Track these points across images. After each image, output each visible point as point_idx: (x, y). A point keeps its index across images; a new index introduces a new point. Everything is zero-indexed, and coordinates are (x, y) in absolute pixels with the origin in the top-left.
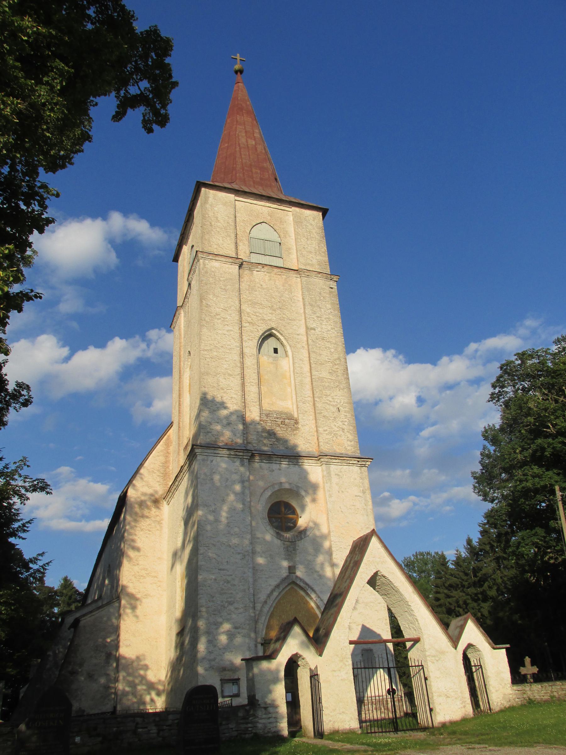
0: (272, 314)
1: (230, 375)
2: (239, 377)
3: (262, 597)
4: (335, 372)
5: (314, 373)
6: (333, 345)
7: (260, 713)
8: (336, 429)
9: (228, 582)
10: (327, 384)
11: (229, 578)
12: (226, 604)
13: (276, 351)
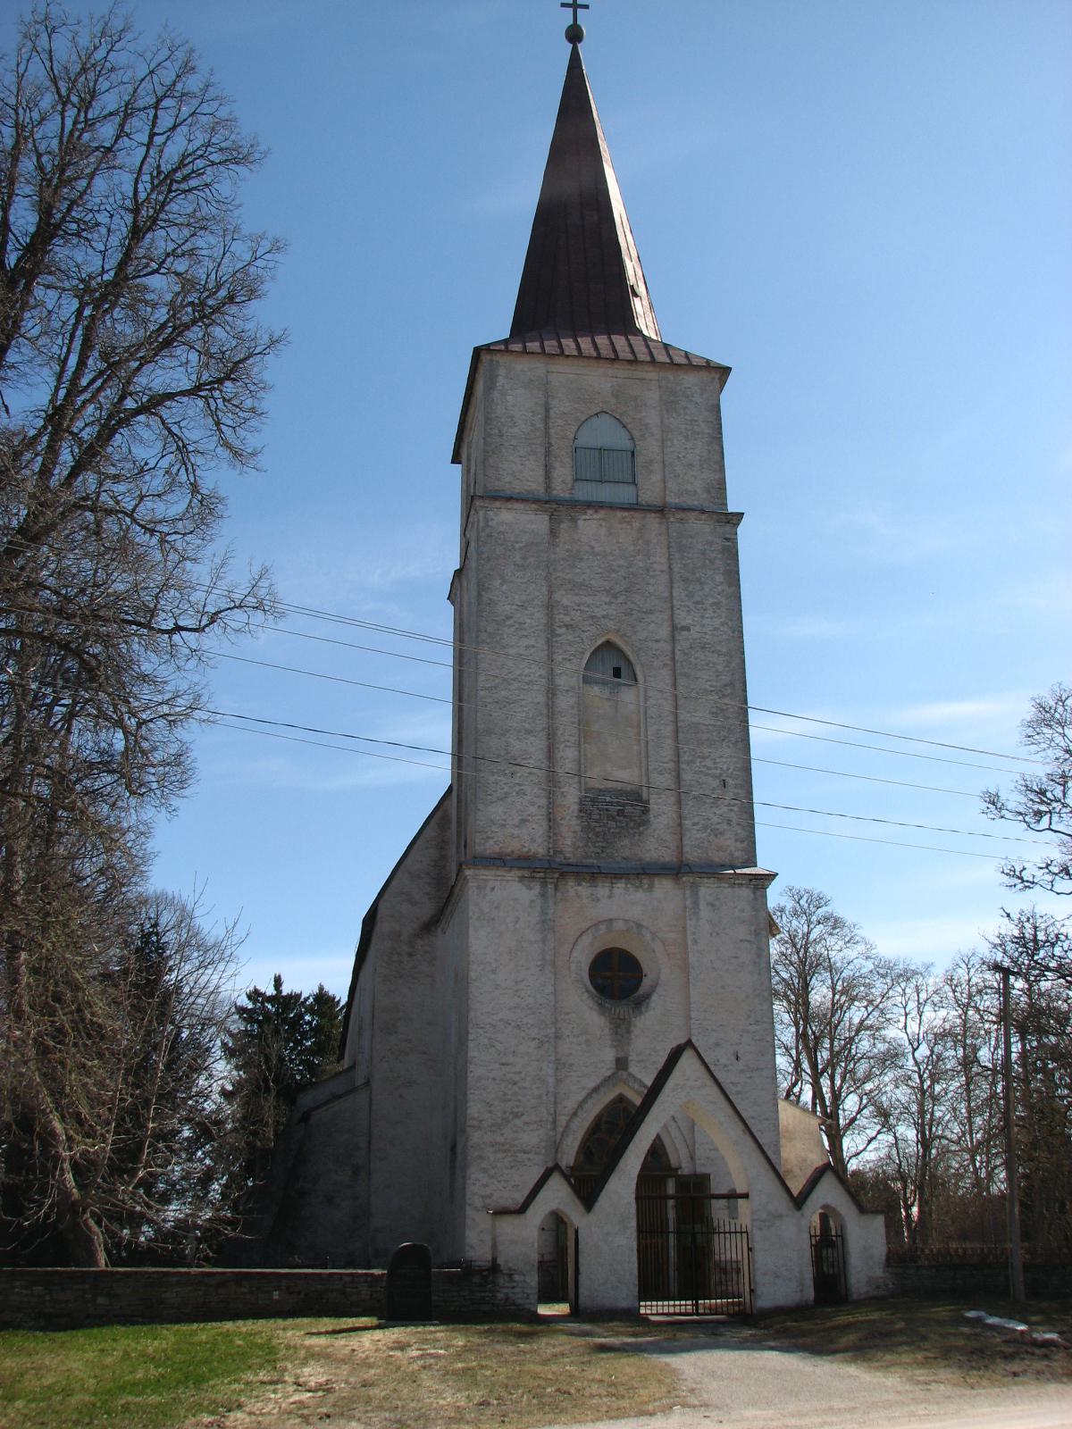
0: (610, 603)
1: (529, 732)
3: (571, 1104)
4: (722, 710)
5: (683, 716)
7: (501, 1280)
9: (515, 1083)
10: (705, 737)
11: (517, 1078)
12: (511, 1117)
13: (617, 673)
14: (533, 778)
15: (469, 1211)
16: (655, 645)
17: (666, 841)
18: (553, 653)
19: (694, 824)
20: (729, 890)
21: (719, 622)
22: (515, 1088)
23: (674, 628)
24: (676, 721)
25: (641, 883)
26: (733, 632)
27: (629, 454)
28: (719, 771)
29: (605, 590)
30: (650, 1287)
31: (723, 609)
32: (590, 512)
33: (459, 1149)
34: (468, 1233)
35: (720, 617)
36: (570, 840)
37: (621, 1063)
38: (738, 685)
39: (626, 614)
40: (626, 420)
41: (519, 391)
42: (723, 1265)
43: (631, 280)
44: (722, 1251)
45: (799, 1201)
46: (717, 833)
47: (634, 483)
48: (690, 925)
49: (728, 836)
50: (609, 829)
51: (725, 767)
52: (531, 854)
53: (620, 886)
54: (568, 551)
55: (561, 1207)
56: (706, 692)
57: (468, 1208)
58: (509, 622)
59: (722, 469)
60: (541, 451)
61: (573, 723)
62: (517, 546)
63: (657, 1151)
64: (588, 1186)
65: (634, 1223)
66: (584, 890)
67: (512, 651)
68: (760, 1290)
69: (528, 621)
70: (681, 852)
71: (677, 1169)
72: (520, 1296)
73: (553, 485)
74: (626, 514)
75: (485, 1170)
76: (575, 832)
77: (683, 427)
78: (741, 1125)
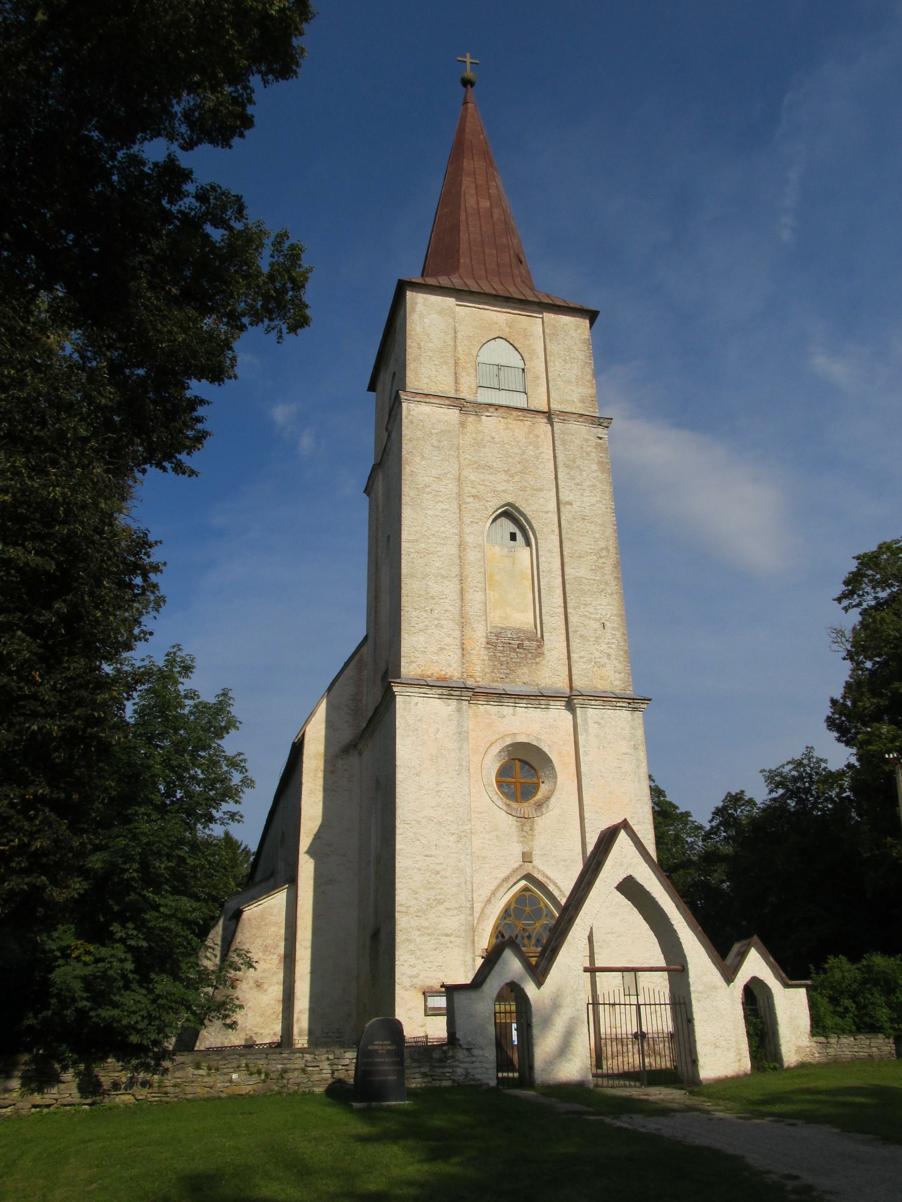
0: (508, 481)
1: (444, 577)
2: (456, 580)
3: (486, 892)
4: (601, 568)
6: (598, 528)
8: (598, 654)
10: (587, 588)
11: (439, 868)
19: (581, 657)
22: (438, 877)
37: (527, 857)
49: (608, 668)
54: (474, 439)
57: (397, 987)
58: (427, 490)
60: (451, 362)
67: (430, 513)
74: (520, 413)
75: (412, 952)
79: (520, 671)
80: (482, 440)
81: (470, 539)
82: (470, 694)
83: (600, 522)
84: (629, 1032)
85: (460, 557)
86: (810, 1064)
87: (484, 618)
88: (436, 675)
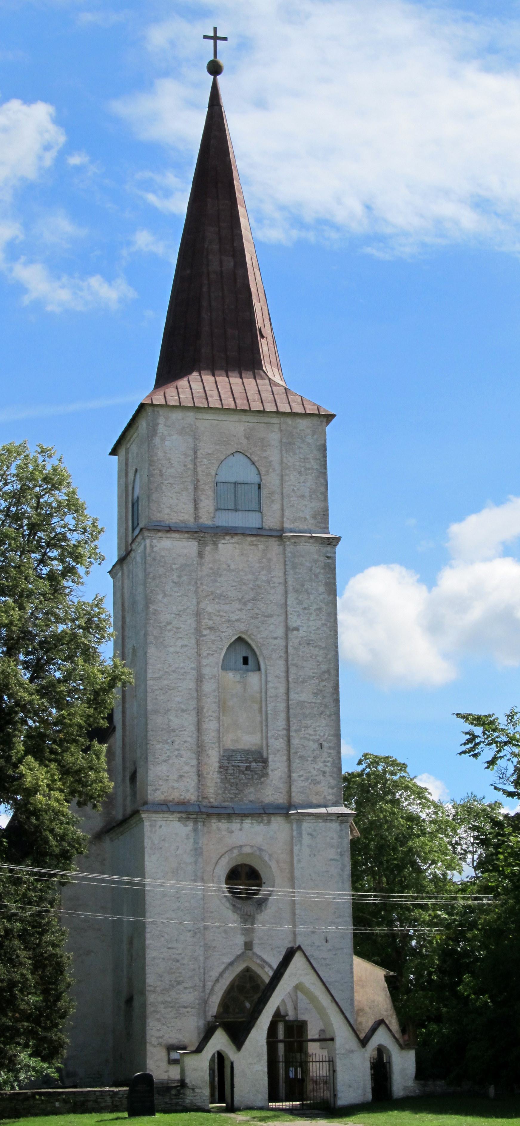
0: (241, 610)
1: (183, 711)
2: (194, 713)
3: (214, 974)
4: (321, 691)
5: (292, 695)
6: (322, 652)
7: (188, 1092)
8: (314, 772)
9: (178, 961)
10: (307, 712)
11: (178, 957)
12: (175, 984)
13: (245, 661)
14: (187, 745)
15: (149, 1048)
16: (274, 642)
17: (280, 788)
18: (201, 649)
19: (300, 776)
20: (323, 824)
21: (320, 623)
22: (178, 964)
23: (287, 629)
24: (288, 700)
25: (262, 820)
26: (331, 631)
27: (257, 486)
28: (318, 737)
29: (238, 599)
30: (273, 1096)
31: (324, 613)
32: (227, 538)
33: (136, 1003)
34: (148, 1061)
35: (320, 619)
36: (213, 789)
37: (248, 946)
38: (333, 672)
39: (253, 618)
40: (255, 458)
41: (174, 437)
42: (315, 1078)
43: (259, 324)
44: (314, 1070)
45: (364, 1043)
46: (316, 783)
47: (260, 511)
48: (296, 849)
49: (322, 784)
50: (240, 780)
51: (322, 734)
52: (186, 800)
53: (248, 823)
54: (211, 568)
55: (223, 1049)
56: (310, 677)
57: (148, 1045)
58: (169, 628)
59: (326, 499)
60: (191, 487)
61: (215, 702)
62: (174, 567)
63: (278, 1017)
64: (238, 1035)
65: (265, 1057)
66: (223, 825)
67: (172, 650)
68: (339, 1095)
69: (183, 626)
70: (290, 796)
71: (285, 1016)
72: (199, 1101)
73: (200, 515)
74: (254, 539)
75: (158, 1020)
76: (216, 783)
77: (298, 464)
78: (330, 998)
79: (246, 791)
80: (219, 569)
81: (206, 671)
82: (205, 816)
83: (323, 645)
84: (321, 1075)
85: (197, 691)
86: (412, 1097)
87: (217, 744)
88: (176, 800)
